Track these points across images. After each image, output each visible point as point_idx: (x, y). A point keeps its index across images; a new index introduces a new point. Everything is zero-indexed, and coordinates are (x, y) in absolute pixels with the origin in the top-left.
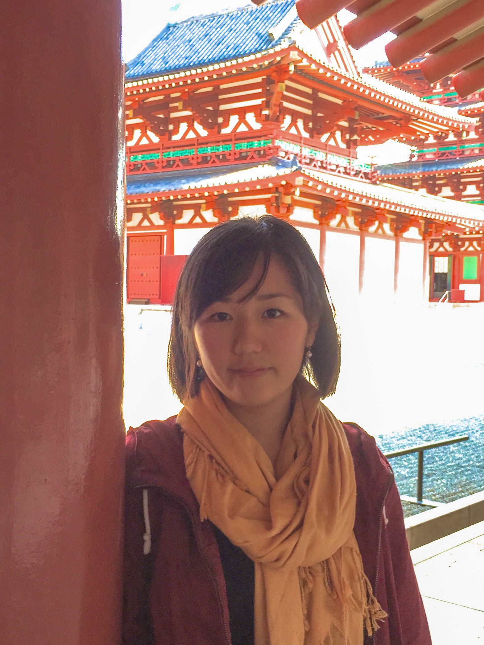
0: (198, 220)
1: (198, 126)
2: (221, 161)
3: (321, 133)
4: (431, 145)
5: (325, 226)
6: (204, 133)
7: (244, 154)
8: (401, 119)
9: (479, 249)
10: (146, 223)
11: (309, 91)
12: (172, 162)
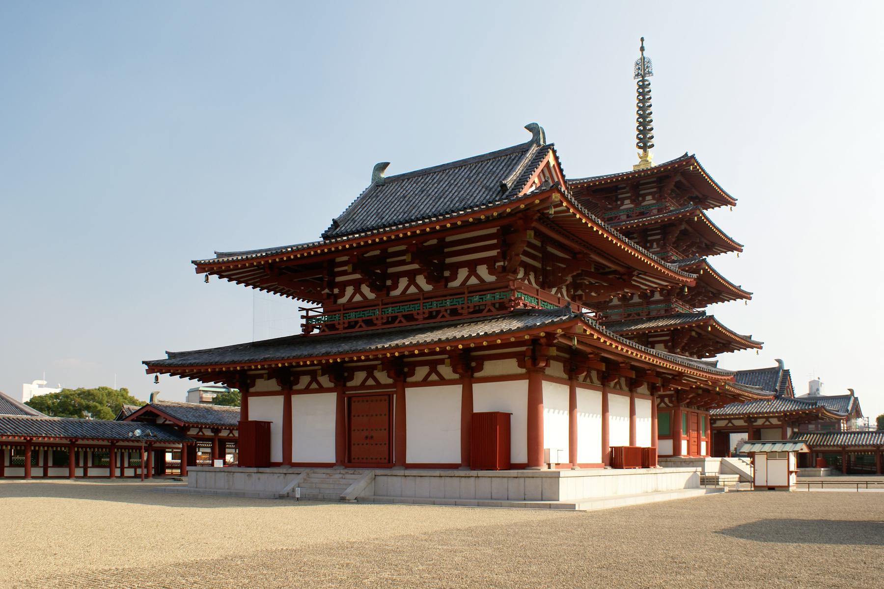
0: (434, 377)
1: (365, 289)
2: (498, 309)
3: (551, 287)
4: (616, 307)
5: (575, 382)
6: (371, 296)
7: (477, 308)
8: (624, 274)
9: (670, 405)
10: (371, 382)
11: (538, 243)
12: (434, 314)
